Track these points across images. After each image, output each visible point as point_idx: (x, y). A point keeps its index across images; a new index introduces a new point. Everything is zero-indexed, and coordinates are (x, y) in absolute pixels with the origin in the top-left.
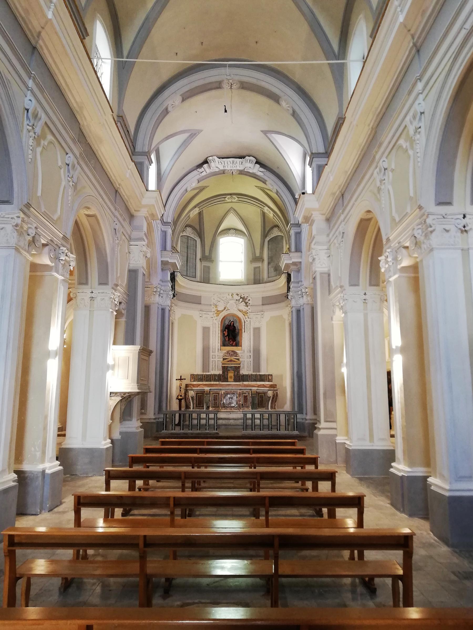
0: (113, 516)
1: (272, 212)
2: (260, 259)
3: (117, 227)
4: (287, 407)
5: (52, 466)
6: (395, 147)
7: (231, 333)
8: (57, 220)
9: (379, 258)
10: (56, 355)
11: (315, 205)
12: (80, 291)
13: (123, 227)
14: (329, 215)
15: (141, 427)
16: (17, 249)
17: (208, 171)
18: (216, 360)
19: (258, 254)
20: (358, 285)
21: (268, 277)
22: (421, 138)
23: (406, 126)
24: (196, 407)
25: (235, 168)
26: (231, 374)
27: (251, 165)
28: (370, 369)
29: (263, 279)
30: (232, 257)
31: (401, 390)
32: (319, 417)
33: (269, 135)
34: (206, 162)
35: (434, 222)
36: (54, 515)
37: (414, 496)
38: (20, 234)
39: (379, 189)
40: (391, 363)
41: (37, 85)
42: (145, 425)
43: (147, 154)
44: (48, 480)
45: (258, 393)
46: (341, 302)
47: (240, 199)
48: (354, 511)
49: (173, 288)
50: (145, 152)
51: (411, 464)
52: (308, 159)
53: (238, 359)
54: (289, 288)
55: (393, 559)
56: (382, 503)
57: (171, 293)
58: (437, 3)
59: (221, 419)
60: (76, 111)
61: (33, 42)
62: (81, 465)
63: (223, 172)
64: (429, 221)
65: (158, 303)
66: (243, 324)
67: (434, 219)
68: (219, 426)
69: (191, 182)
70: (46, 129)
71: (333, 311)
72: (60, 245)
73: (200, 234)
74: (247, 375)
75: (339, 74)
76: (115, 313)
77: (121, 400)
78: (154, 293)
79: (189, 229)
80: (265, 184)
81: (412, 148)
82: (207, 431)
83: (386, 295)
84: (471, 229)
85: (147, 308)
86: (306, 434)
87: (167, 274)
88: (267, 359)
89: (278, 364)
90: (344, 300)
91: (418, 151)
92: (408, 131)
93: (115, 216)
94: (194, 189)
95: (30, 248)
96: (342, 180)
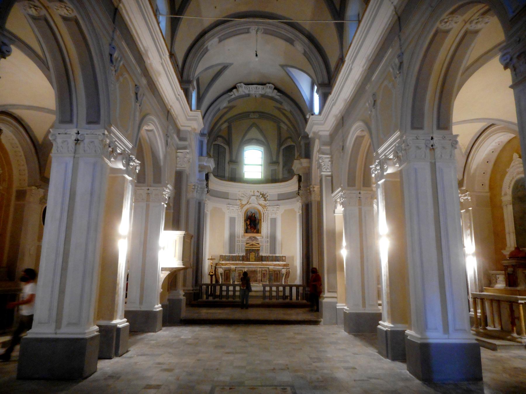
7: (252, 223)
18: (240, 244)
19: (274, 159)
30: (253, 161)
33: (285, 68)
34: (235, 87)
45: (275, 271)
51: (393, 321)
52: (316, 88)
53: (258, 244)
57: (206, 190)
69: (224, 104)
94: (225, 108)
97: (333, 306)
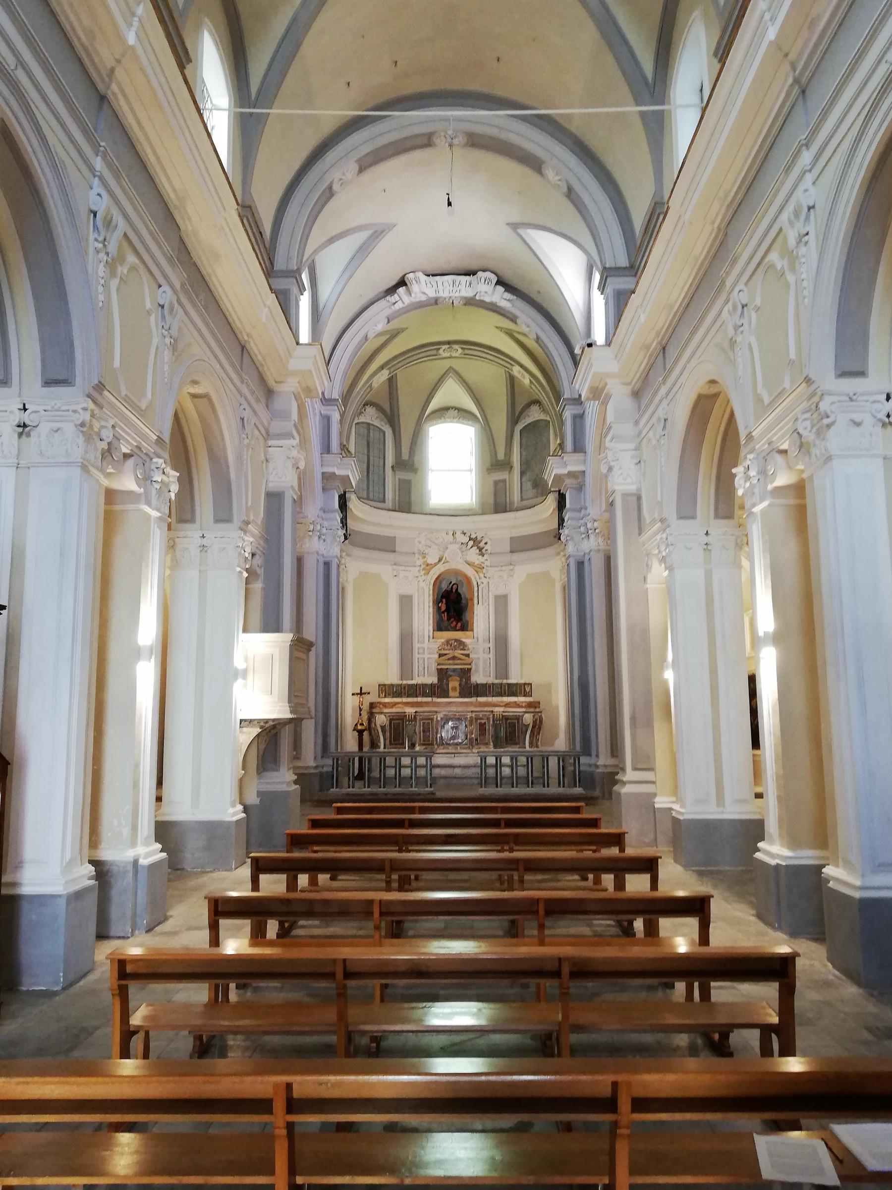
0: (264, 935)
1: (527, 376)
3: (247, 414)
5: (149, 853)
6: (761, 267)
7: (452, 606)
8: (147, 407)
9: (734, 471)
10: (151, 654)
11: (613, 367)
12: (182, 534)
15: (296, 782)
16: (84, 468)
17: (407, 300)
18: (426, 656)
19: (501, 456)
20: (694, 517)
21: (522, 500)
22: (810, 253)
23: (781, 230)
24: (391, 744)
25: (457, 295)
26: (454, 683)
27: (489, 288)
28: (717, 671)
29: (512, 503)
30: (452, 461)
31: (774, 712)
33: (521, 231)
34: (402, 283)
36: (157, 938)
37: (802, 898)
38: (88, 438)
39: (732, 343)
40: (756, 659)
41: (110, 166)
42: (302, 778)
43: (295, 275)
44: (143, 876)
45: (506, 718)
46: (663, 548)
48: (692, 923)
49: (344, 522)
51: (794, 842)
52: (597, 277)
53: (468, 655)
54: (561, 521)
55: (761, 997)
56: (739, 914)
57: (341, 533)
58: (838, 6)
59: (438, 766)
60: (175, 206)
61: (101, 87)
62: (193, 850)
63: (436, 301)
64: (823, 406)
65: (317, 553)
66: (476, 589)
67: (833, 403)
68: (434, 780)
69: (375, 323)
70: (125, 244)
71: (647, 565)
72: (152, 455)
73: (392, 419)
75: (657, 128)
76: (245, 575)
77: (258, 735)
78: (311, 533)
79: (370, 410)
80: (516, 323)
81: (793, 269)
82: (414, 789)
83: (747, 535)
85: (299, 562)
86: (597, 793)
87: (334, 497)
88: (522, 654)
90: (667, 545)
91: (804, 276)
95: (104, 463)
96: (663, 321)
97: (646, 802)
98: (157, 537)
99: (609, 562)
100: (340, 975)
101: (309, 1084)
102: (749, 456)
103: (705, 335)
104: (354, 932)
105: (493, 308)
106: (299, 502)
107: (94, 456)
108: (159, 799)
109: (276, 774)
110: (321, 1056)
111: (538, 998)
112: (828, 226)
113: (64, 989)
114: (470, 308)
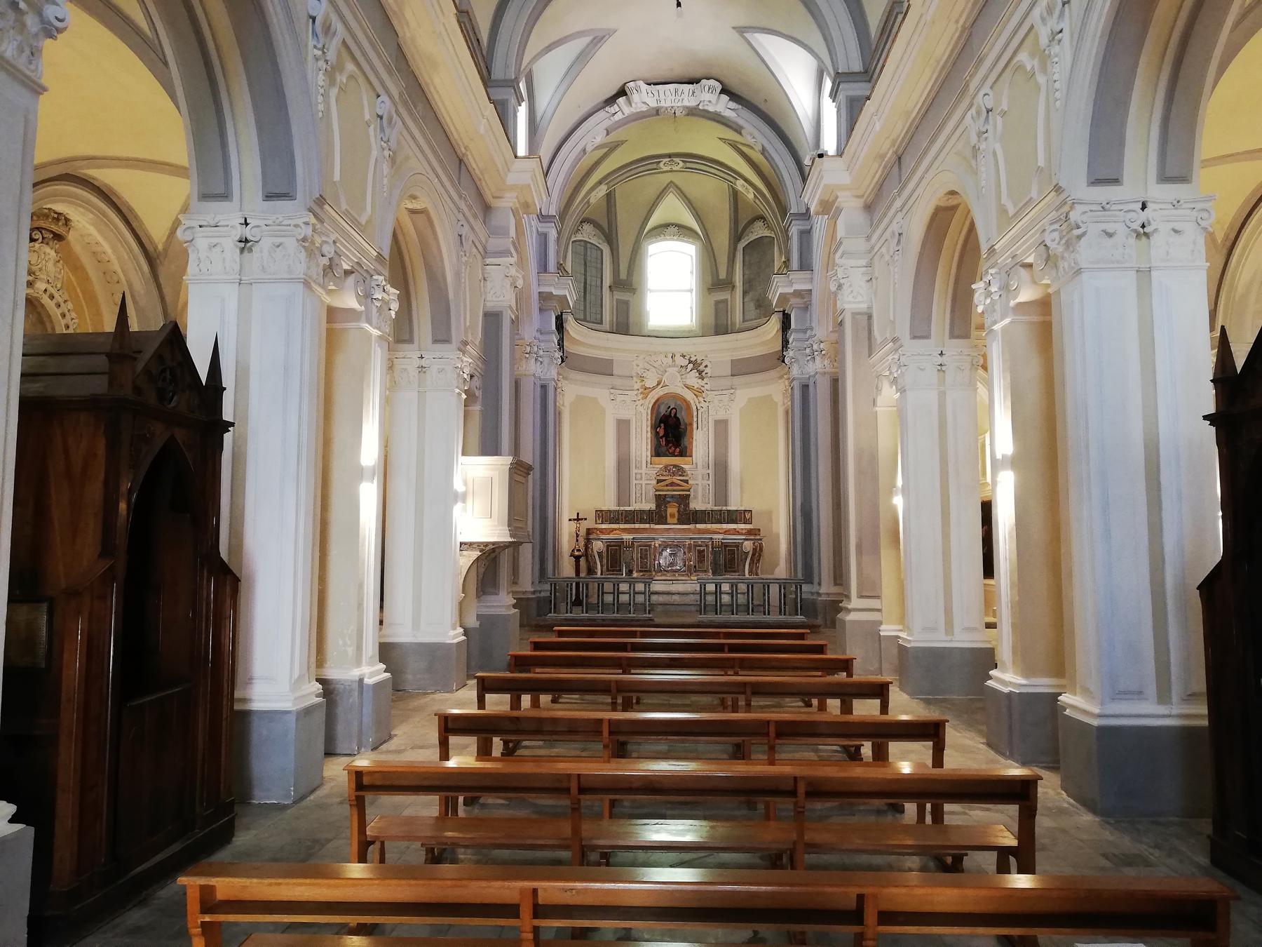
1: (751, 190)
2: (728, 284)
3: (465, 231)
4: (781, 571)
5: (374, 673)
7: (671, 431)
8: (367, 222)
9: (973, 286)
11: (844, 178)
12: (401, 354)
13: (472, 228)
14: (872, 196)
15: (515, 606)
16: (306, 284)
18: (644, 482)
20: (928, 337)
22: (1063, 53)
23: (1032, 27)
26: (672, 510)
27: (713, 97)
29: (733, 324)
30: (671, 282)
31: (1010, 537)
32: (848, 588)
34: (622, 92)
35: (1085, 218)
38: (310, 253)
39: (975, 150)
42: (521, 603)
43: (512, 84)
44: (368, 696)
47: (689, 165)
50: (512, 81)
51: (1028, 671)
52: (828, 85)
53: (686, 482)
54: (785, 343)
56: (968, 742)
57: (558, 355)
62: (414, 672)
63: (657, 112)
64: (1074, 216)
68: (653, 607)
69: (594, 134)
70: (343, 50)
73: (610, 236)
74: (703, 512)
76: (464, 396)
79: (588, 228)
81: (1044, 69)
84: (1156, 230)
85: (517, 385)
86: (819, 621)
89: (762, 488)
90: (900, 366)
91: (1056, 77)
92: (1037, 37)
93: (459, 209)
94: (597, 148)
96: (900, 128)
98: (378, 358)
99: (836, 386)
100: (574, 790)
101: (553, 890)
102: (990, 271)
103: (948, 139)
104: (578, 753)
105: (717, 118)
106: (515, 323)
107: (316, 272)
108: (381, 622)
109: (493, 597)
110: (555, 869)
111: (767, 817)
112: (1084, 24)
113: (295, 802)
114: (694, 119)
